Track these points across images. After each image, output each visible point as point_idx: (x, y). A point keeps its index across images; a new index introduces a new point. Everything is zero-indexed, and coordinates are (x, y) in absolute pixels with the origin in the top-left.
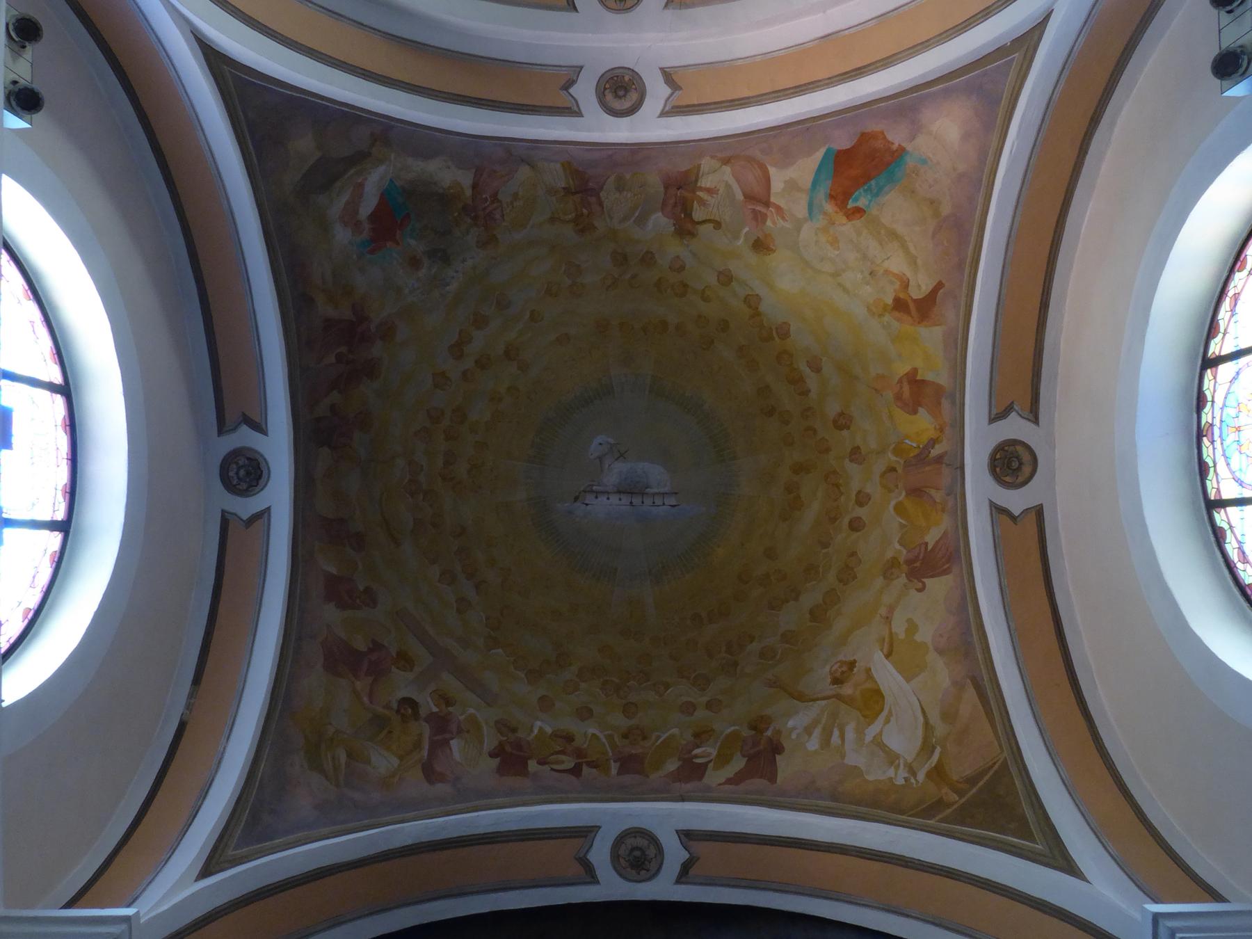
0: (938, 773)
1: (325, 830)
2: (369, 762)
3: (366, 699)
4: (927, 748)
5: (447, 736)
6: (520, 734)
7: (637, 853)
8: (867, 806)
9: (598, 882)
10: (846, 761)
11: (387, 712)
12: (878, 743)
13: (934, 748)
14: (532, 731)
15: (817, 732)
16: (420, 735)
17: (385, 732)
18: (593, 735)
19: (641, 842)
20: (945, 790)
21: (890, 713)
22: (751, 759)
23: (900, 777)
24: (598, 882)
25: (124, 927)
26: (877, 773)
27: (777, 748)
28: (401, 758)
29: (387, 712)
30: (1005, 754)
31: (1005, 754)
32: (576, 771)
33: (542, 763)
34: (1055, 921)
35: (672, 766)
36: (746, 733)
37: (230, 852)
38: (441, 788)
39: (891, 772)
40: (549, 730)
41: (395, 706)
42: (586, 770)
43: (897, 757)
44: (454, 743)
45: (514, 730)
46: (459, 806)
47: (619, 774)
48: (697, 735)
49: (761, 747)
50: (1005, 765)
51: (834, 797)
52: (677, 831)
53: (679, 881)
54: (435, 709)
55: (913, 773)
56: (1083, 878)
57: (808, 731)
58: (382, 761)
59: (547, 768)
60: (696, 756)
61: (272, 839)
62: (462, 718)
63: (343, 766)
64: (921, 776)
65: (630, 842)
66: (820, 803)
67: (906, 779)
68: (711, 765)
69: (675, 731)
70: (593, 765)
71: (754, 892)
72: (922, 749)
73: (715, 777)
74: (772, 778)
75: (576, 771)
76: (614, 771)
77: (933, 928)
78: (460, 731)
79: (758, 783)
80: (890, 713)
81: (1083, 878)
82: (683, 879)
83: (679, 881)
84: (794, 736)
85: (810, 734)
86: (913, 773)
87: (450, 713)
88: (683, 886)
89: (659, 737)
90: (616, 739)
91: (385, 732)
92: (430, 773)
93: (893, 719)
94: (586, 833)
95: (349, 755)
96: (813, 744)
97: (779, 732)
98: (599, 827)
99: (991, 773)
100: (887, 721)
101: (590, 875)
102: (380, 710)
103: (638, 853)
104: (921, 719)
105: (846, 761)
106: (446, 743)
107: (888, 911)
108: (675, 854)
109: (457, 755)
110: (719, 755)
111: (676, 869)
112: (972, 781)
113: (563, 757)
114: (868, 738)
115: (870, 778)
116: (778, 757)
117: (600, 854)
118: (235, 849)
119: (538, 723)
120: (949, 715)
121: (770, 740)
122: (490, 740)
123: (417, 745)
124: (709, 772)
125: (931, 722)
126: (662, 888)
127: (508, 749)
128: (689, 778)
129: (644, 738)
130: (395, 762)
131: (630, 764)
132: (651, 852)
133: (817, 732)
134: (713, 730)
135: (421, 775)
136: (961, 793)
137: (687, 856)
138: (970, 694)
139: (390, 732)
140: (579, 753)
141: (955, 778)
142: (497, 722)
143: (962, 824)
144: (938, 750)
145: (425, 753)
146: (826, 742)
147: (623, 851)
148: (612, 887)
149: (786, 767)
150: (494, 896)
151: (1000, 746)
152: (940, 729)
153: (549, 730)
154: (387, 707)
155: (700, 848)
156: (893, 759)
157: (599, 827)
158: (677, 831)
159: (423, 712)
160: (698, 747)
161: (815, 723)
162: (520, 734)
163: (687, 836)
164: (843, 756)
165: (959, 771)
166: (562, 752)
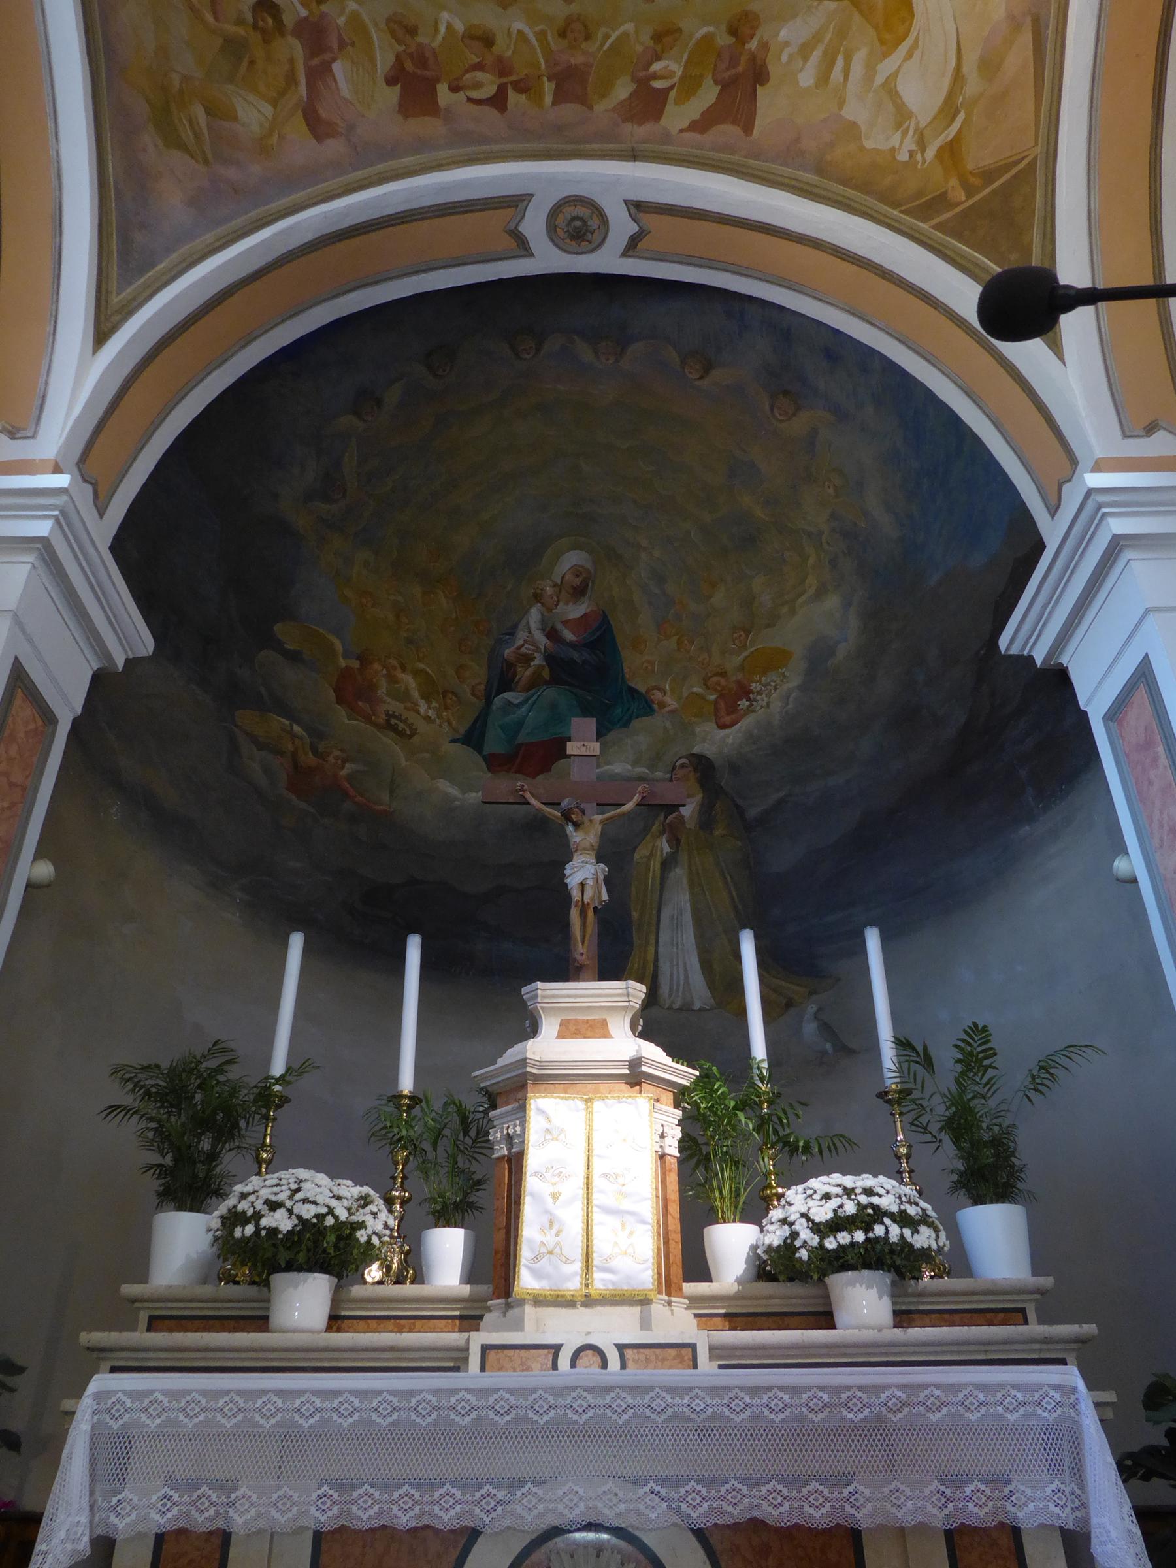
0: (952, 152)
1: (209, 237)
2: (235, 118)
3: (209, 18)
4: (949, 110)
5: (327, 56)
6: (421, 39)
7: (578, 223)
8: (856, 188)
9: (532, 255)
10: (843, 113)
11: (240, 31)
12: (890, 89)
13: (957, 112)
14: (437, 30)
15: (817, 55)
16: (292, 61)
17: (245, 64)
18: (520, 32)
19: (581, 211)
20: (954, 182)
21: (916, 41)
22: (727, 87)
23: (904, 147)
24: (532, 255)
25: (65, 498)
26: (882, 139)
27: (759, 75)
28: (274, 103)
29: (240, 31)
30: (1039, 149)
31: (1039, 149)
32: (498, 101)
33: (455, 89)
34: (1017, 387)
35: (623, 90)
36: (724, 40)
37: (115, 300)
38: (334, 147)
39: (895, 140)
40: (460, 27)
41: (249, 18)
42: (513, 97)
43: (909, 115)
44: (337, 67)
45: (412, 31)
46: (360, 174)
47: (555, 102)
48: (658, 37)
49: (740, 69)
50: (1032, 165)
51: (820, 170)
52: (625, 202)
53: (625, 254)
54: (304, 13)
55: (922, 145)
56: (1061, 358)
57: (805, 51)
58: (252, 113)
59: (461, 96)
60: (655, 76)
61: (153, 265)
62: (341, 21)
63: (205, 131)
64: (930, 153)
65: (570, 211)
66: (801, 174)
67: (911, 153)
68: (673, 94)
69: (629, 27)
70: (522, 87)
71: (707, 271)
72: (941, 110)
73: (678, 116)
74: (748, 128)
75: (498, 101)
76: (548, 99)
77: (897, 343)
78: (342, 45)
79: (728, 132)
80: (916, 41)
81: (1061, 358)
82: (631, 253)
83: (625, 254)
84: (784, 58)
85: (806, 59)
86: (922, 145)
87: (323, 15)
88: (631, 260)
89: (607, 36)
90: (550, 38)
91: (245, 64)
92: (318, 128)
93: (917, 53)
94: (516, 203)
95: (208, 112)
96: (807, 78)
97: (765, 46)
98: (532, 195)
99: (1014, 171)
100: (909, 55)
101: (523, 247)
102: (231, 29)
103: (578, 222)
104: (953, 63)
105: (843, 113)
106: (326, 68)
107: (854, 314)
108: (622, 226)
109: (345, 89)
110: (683, 78)
111: (624, 242)
112: (988, 176)
113: (480, 76)
114: (879, 80)
115: (869, 144)
116: (759, 89)
117: (534, 225)
118: (118, 294)
119: (445, 16)
120: (990, 66)
121: (753, 58)
122: (384, 60)
123: (291, 79)
124: (670, 108)
125: (965, 69)
126: (607, 260)
127: (409, 66)
128: (640, 120)
129: (588, 37)
130: (268, 110)
131: (571, 84)
132: (594, 223)
133: (817, 55)
134: (680, 30)
135: (304, 127)
136: (970, 191)
137: (636, 229)
138: (1027, 37)
139: (252, 62)
140: (502, 68)
141: (970, 166)
142: (389, 20)
143: (959, 237)
144: (961, 117)
145: (303, 90)
146: (824, 78)
147: (561, 220)
148: (547, 259)
149: (770, 106)
150: (414, 278)
151: (1037, 136)
152: (973, 85)
153: (460, 27)
154: (240, 22)
155: (650, 220)
156: (902, 115)
157: (532, 195)
158: (625, 202)
159: (288, 20)
160: (658, 58)
161: (817, 38)
162: (421, 39)
163: (637, 207)
164: (842, 102)
165: (977, 157)
166: (479, 67)
